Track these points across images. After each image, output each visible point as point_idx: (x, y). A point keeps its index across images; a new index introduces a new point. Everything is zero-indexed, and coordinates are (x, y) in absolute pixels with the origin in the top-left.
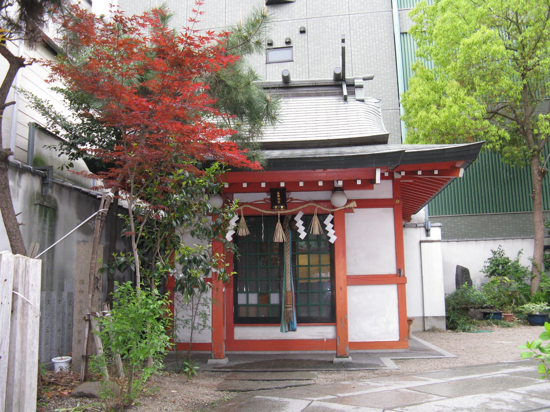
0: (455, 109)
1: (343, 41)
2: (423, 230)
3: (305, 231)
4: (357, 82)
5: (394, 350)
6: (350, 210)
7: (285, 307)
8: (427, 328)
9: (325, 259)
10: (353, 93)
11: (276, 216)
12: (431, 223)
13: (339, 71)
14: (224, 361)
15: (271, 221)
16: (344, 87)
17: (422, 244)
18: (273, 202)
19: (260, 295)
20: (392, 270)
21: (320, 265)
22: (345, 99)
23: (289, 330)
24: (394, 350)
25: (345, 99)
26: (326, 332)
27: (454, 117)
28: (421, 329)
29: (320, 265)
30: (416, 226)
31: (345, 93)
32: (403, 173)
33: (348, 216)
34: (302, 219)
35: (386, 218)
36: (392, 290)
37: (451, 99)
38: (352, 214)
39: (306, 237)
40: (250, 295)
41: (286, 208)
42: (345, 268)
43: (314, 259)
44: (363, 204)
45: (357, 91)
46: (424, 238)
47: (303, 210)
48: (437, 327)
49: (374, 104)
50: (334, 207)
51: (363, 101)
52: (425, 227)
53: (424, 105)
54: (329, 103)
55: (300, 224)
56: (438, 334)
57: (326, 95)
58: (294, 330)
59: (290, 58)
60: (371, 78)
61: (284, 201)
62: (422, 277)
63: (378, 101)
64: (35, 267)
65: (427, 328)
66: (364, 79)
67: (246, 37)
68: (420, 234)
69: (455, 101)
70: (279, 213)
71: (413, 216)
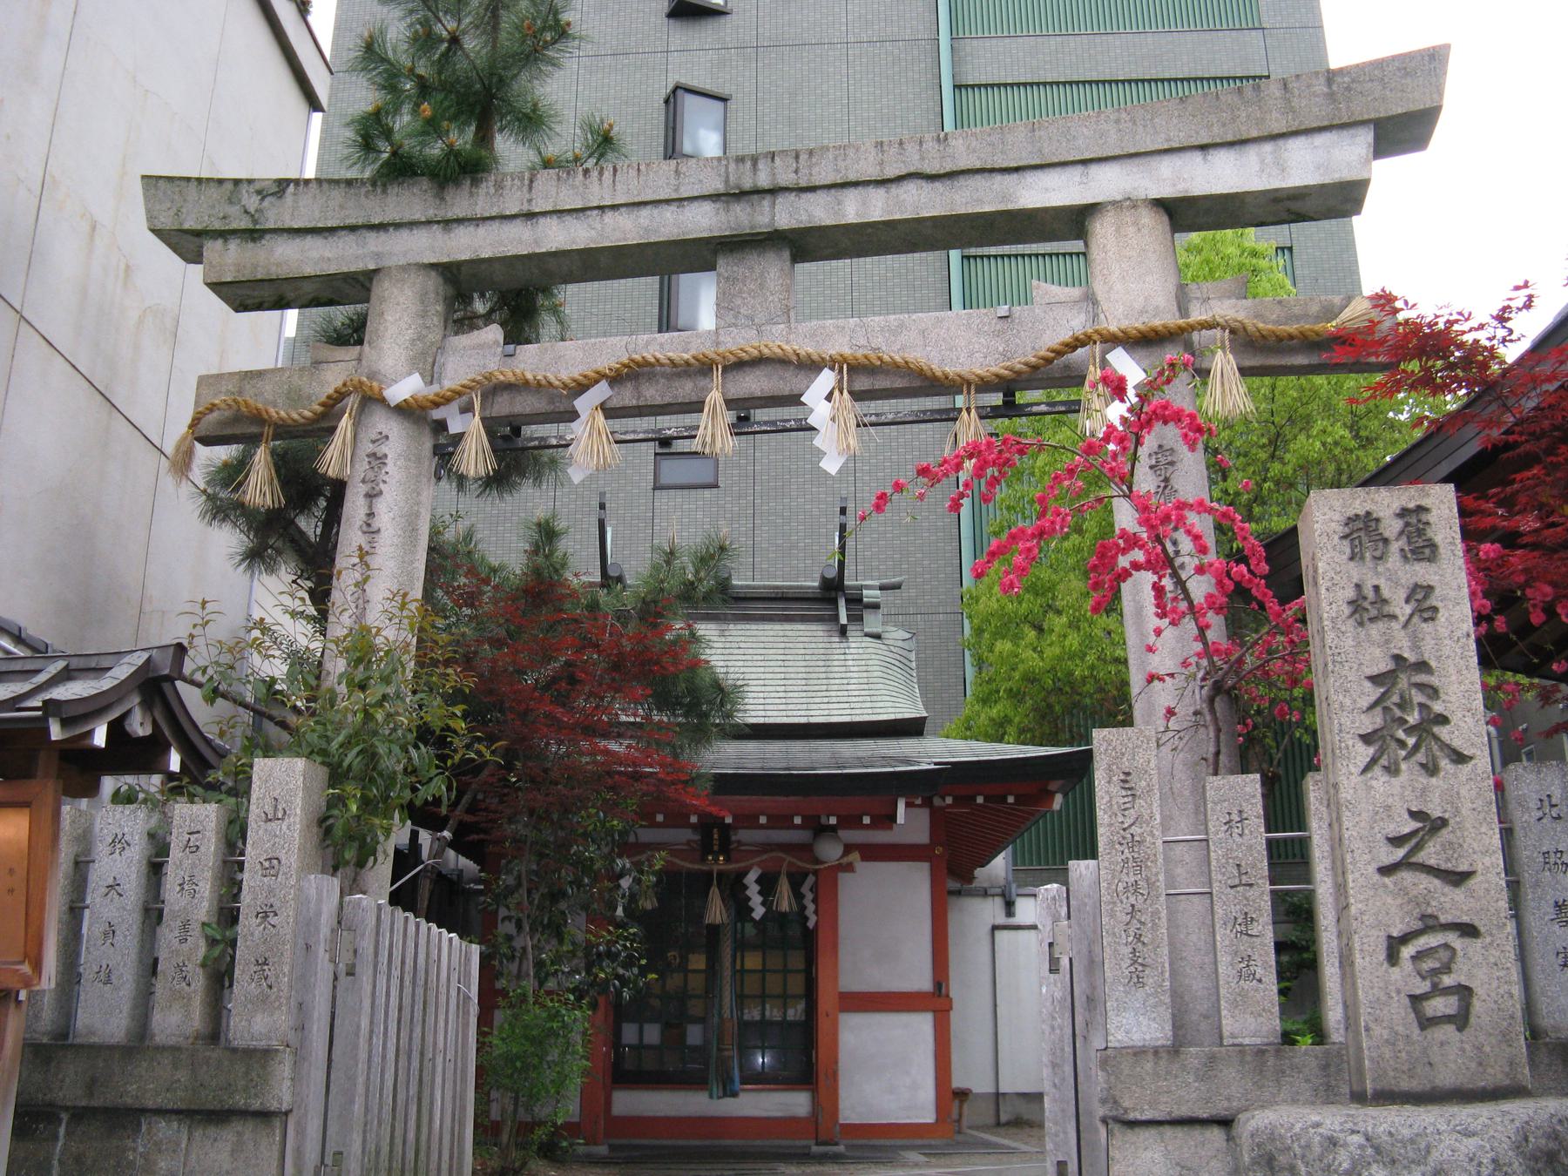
0: (1073, 641)
1: (843, 511)
2: (999, 901)
3: (763, 904)
4: (870, 595)
5: (925, 1142)
6: (849, 868)
7: (719, 1049)
8: (1004, 1118)
9: (797, 960)
10: (860, 619)
11: (710, 873)
12: (1019, 886)
13: (832, 573)
14: (602, 1150)
15: (702, 882)
16: (842, 603)
17: (998, 934)
18: (706, 848)
19: (667, 1026)
20: (920, 979)
21: (785, 971)
22: (843, 632)
23: (725, 1095)
24: (925, 1142)
25: (843, 632)
26: (797, 1103)
27: (1071, 658)
28: (991, 1120)
29: (785, 971)
30: (985, 894)
31: (843, 620)
32: (949, 800)
33: (843, 878)
34: (758, 881)
35: (915, 882)
36: (923, 1023)
37: (1064, 619)
38: (666, 10)
39: (764, 916)
40: (647, 1027)
41: (727, 860)
42: (836, 979)
43: (775, 961)
44: (873, 853)
45: (869, 617)
46: (1001, 919)
47: (759, 865)
48: (1025, 1117)
49: (900, 644)
50: (818, 861)
51: (878, 637)
52: (1003, 895)
53: (1007, 626)
54: (807, 637)
55: (753, 891)
56: (1028, 1130)
57: (804, 619)
58: (734, 1095)
59: (710, 480)
60: (897, 587)
61: (725, 848)
62: (995, 1005)
63: (908, 636)
64: (475, 949)
65: (1004, 1118)
66: (882, 588)
67: (692, 583)
68: (992, 910)
69: (1074, 625)
70: (715, 868)
71: (978, 872)
